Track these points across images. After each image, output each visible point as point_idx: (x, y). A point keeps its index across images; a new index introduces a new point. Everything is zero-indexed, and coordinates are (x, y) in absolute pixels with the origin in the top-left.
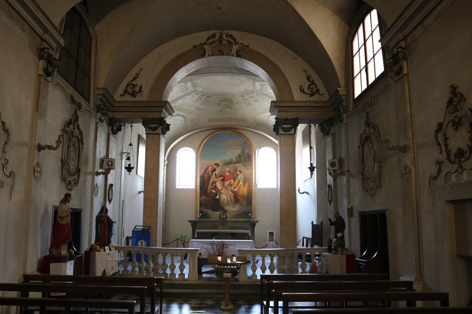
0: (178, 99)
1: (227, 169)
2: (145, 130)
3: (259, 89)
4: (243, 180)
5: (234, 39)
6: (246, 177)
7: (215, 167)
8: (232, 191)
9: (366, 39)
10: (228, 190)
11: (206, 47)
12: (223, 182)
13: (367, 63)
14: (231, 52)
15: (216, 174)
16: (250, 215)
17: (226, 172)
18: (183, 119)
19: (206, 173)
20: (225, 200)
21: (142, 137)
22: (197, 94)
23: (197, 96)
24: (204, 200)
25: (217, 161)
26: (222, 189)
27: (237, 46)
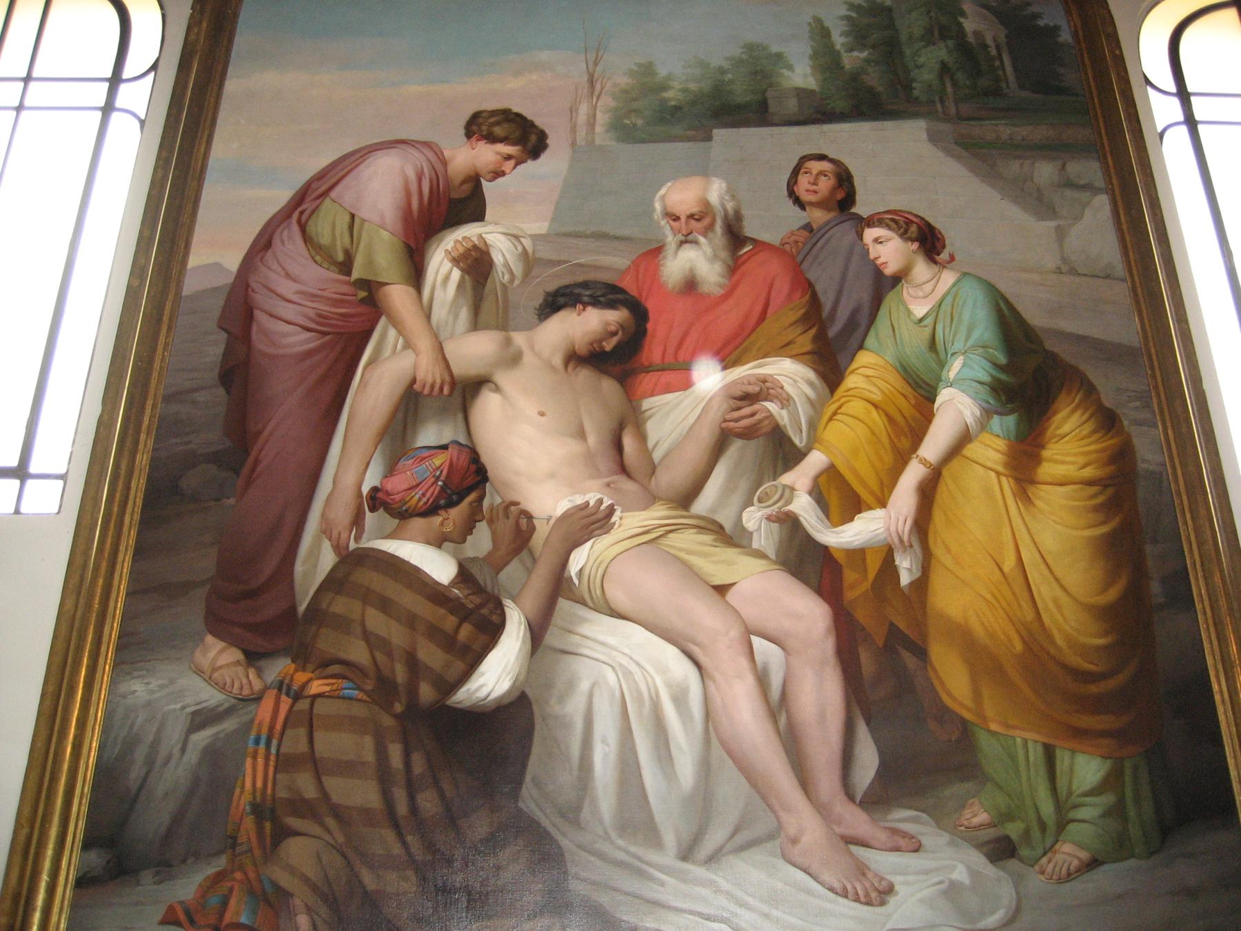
4: (982, 371)
6: (1035, 317)
12: (609, 386)
17: (671, 240)
24: (202, 738)
25: (514, 84)
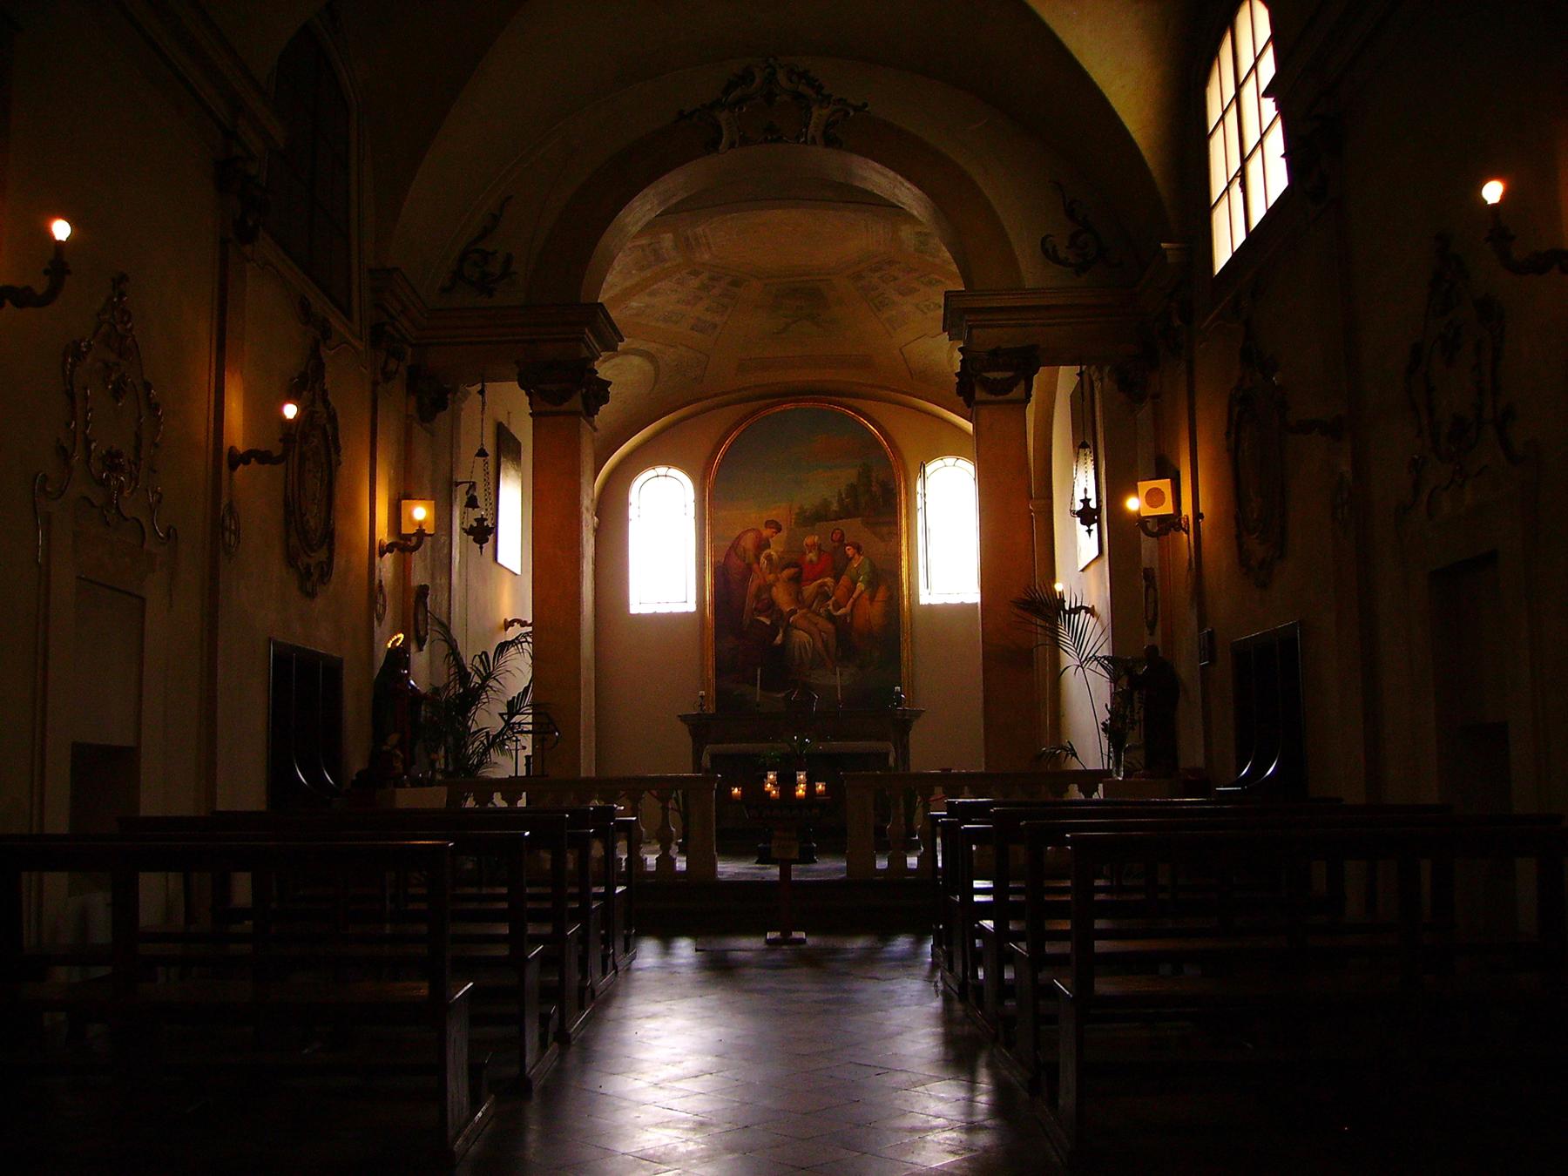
0: (628, 293)
1: (809, 540)
2: (530, 404)
3: (912, 249)
5: (817, 84)
7: (766, 532)
8: (831, 618)
9: (1241, 80)
10: (814, 612)
11: (723, 116)
13: (1244, 160)
14: (807, 131)
15: (769, 557)
16: (897, 692)
18: (647, 366)
19: (736, 554)
20: (805, 648)
21: (508, 431)
22: (696, 274)
23: (694, 283)
26: (793, 612)
27: (827, 107)
